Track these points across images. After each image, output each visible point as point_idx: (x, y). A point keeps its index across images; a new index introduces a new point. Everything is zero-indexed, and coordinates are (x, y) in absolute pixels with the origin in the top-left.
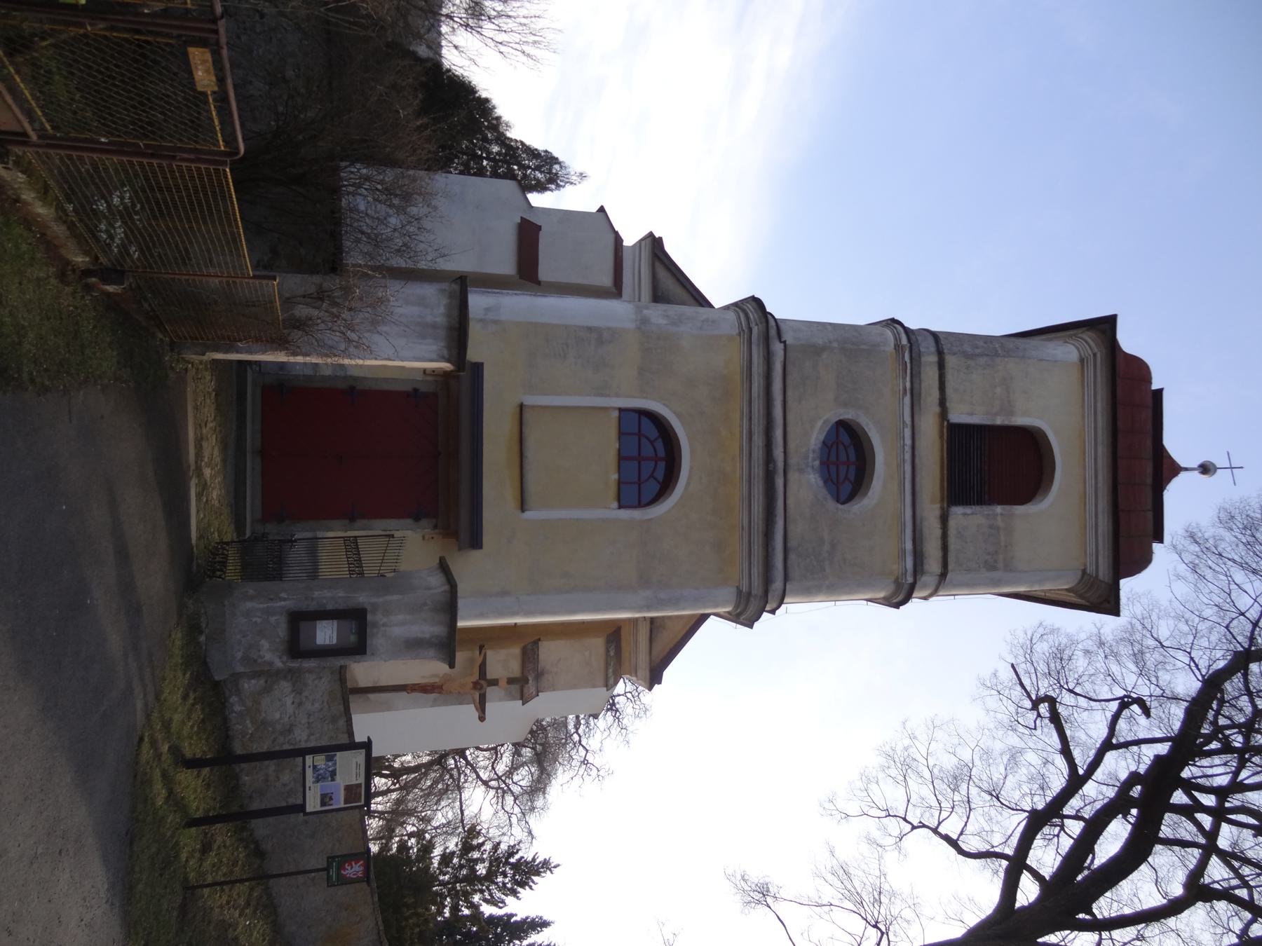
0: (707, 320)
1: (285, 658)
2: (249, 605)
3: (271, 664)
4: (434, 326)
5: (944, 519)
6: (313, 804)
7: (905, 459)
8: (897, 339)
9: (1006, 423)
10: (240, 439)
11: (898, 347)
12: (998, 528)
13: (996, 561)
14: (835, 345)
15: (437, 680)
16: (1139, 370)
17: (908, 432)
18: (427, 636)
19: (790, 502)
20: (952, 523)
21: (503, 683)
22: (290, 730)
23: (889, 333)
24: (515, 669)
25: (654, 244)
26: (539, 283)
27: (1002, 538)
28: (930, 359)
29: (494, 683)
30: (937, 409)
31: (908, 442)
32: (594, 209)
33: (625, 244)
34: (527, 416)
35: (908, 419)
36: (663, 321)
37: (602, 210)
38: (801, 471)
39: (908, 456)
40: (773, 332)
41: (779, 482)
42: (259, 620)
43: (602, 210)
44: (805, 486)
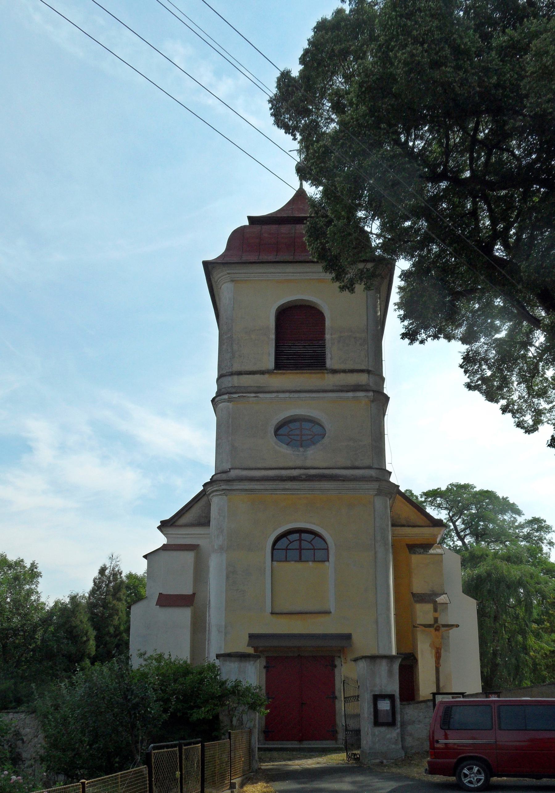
1: (396, 728)
3: (398, 734)
5: (334, 372)
7: (298, 395)
8: (224, 401)
9: (274, 331)
10: (293, 750)
11: (229, 400)
15: (434, 651)
16: (238, 238)
17: (281, 395)
18: (387, 668)
19: (325, 465)
20: (336, 367)
23: (221, 405)
24: (429, 607)
25: (164, 526)
26: (194, 594)
28: (236, 381)
29: (436, 620)
30: (267, 376)
31: (287, 395)
32: (146, 561)
33: (166, 543)
35: (274, 395)
37: (145, 557)
39: (296, 395)
40: (224, 476)
41: (312, 472)
42: (377, 739)
43: (145, 557)
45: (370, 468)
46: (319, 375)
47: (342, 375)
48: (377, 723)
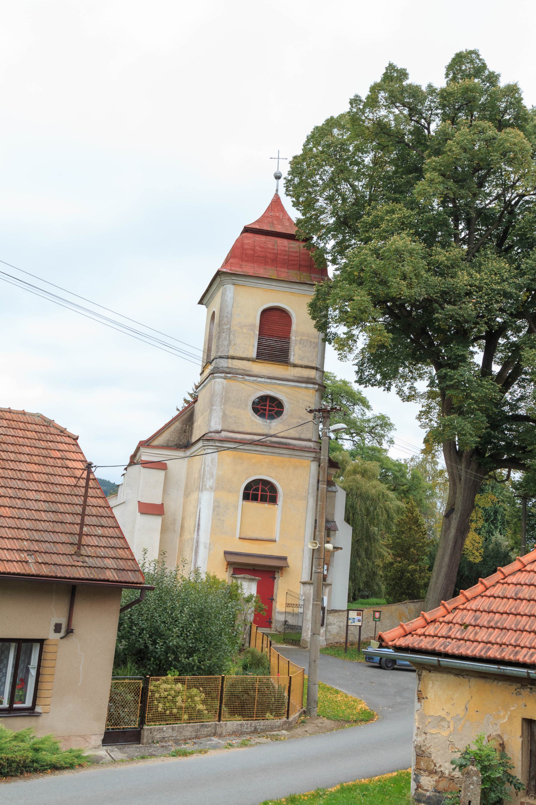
0: (211, 462)
4: (248, 585)
5: (295, 366)
6: (360, 624)
12: (301, 340)
13: (314, 343)
14: (222, 407)
17: (259, 379)
20: (297, 362)
22: (340, 627)
27: (305, 338)
30: (250, 363)
34: (243, 536)
36: (212, 481)
38: (270, 429)
44: (275, 427)
45: (310, 440)
46: (285, 367)
47: (300, 369)
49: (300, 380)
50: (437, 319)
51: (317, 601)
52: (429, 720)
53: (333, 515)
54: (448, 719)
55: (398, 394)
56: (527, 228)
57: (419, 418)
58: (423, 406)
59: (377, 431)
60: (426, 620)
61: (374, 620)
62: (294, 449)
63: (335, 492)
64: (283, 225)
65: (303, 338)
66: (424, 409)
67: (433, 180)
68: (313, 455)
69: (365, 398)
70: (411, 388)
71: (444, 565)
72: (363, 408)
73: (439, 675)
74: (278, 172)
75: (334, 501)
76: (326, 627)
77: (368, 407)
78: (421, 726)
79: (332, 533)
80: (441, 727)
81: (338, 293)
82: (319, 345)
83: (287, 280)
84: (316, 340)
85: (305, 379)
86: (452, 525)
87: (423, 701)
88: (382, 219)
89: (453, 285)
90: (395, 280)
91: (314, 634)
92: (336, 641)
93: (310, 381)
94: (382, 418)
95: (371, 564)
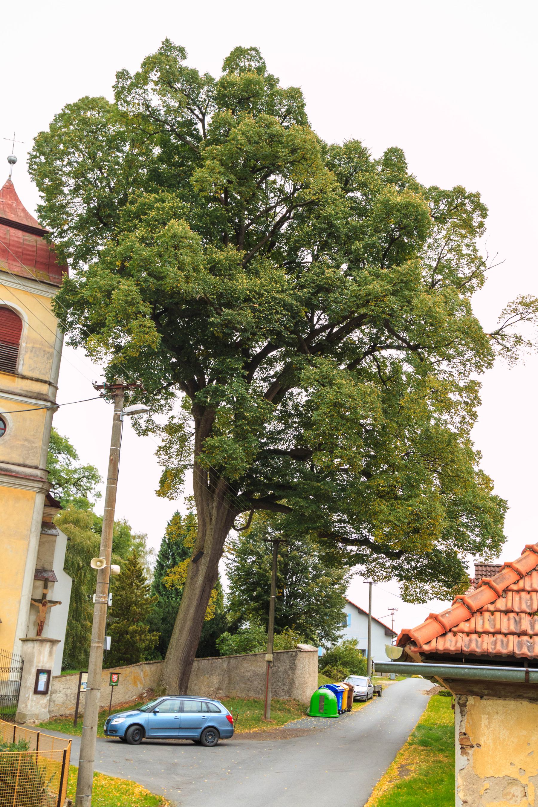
2: (29, 707)
5: (24, 377)
12: (33, 347)
13: (48, 353)
21: (45, 591)
22: (67, 695)
27: (38, 346)
29: (44, 596)
45: (36, 468)
46: (11, 377)
47: (29, 382)
48: (36, 692)
49: (29, 394)
50: (212, 324)
51: (98, 642)
52: (487, 784)
53: (51, 563)
54: (523, 780)
55: (133, 426)
56: (305, 241)
57: (158, 454)
58: (163, 441)
59: (82, 483)
60: (469, 607)
61: (110, 685)
62: (17, 477)
63: (56, 536)
64: (16, 214)
65: (35, 346)
66: (164, 444)
67: (214, 169)
68: (40, 485)
69: (71, 447)
70: (148, 421)
71: (189, 618)
72: (69, 457)
73: (500, 702)
74: (13, 155)
75: (54, 547)
76: (51, 696)
77: (75, 457)
78: (469, 799)
79: (50, 584)
80: (508, 797)
81: (98, 282)
82: (55, 355)
83: (21, 275)
84: (51, 350)
85: (35, 395)
86: (200, 572)
87: (471, 751)
88: (151, 208)
89: (231, 287)
90: (171, 269)
91: (92, 689)
92: (61, 713)
93: (41, 397)
94: (90, 469)
95: (79, 626)
